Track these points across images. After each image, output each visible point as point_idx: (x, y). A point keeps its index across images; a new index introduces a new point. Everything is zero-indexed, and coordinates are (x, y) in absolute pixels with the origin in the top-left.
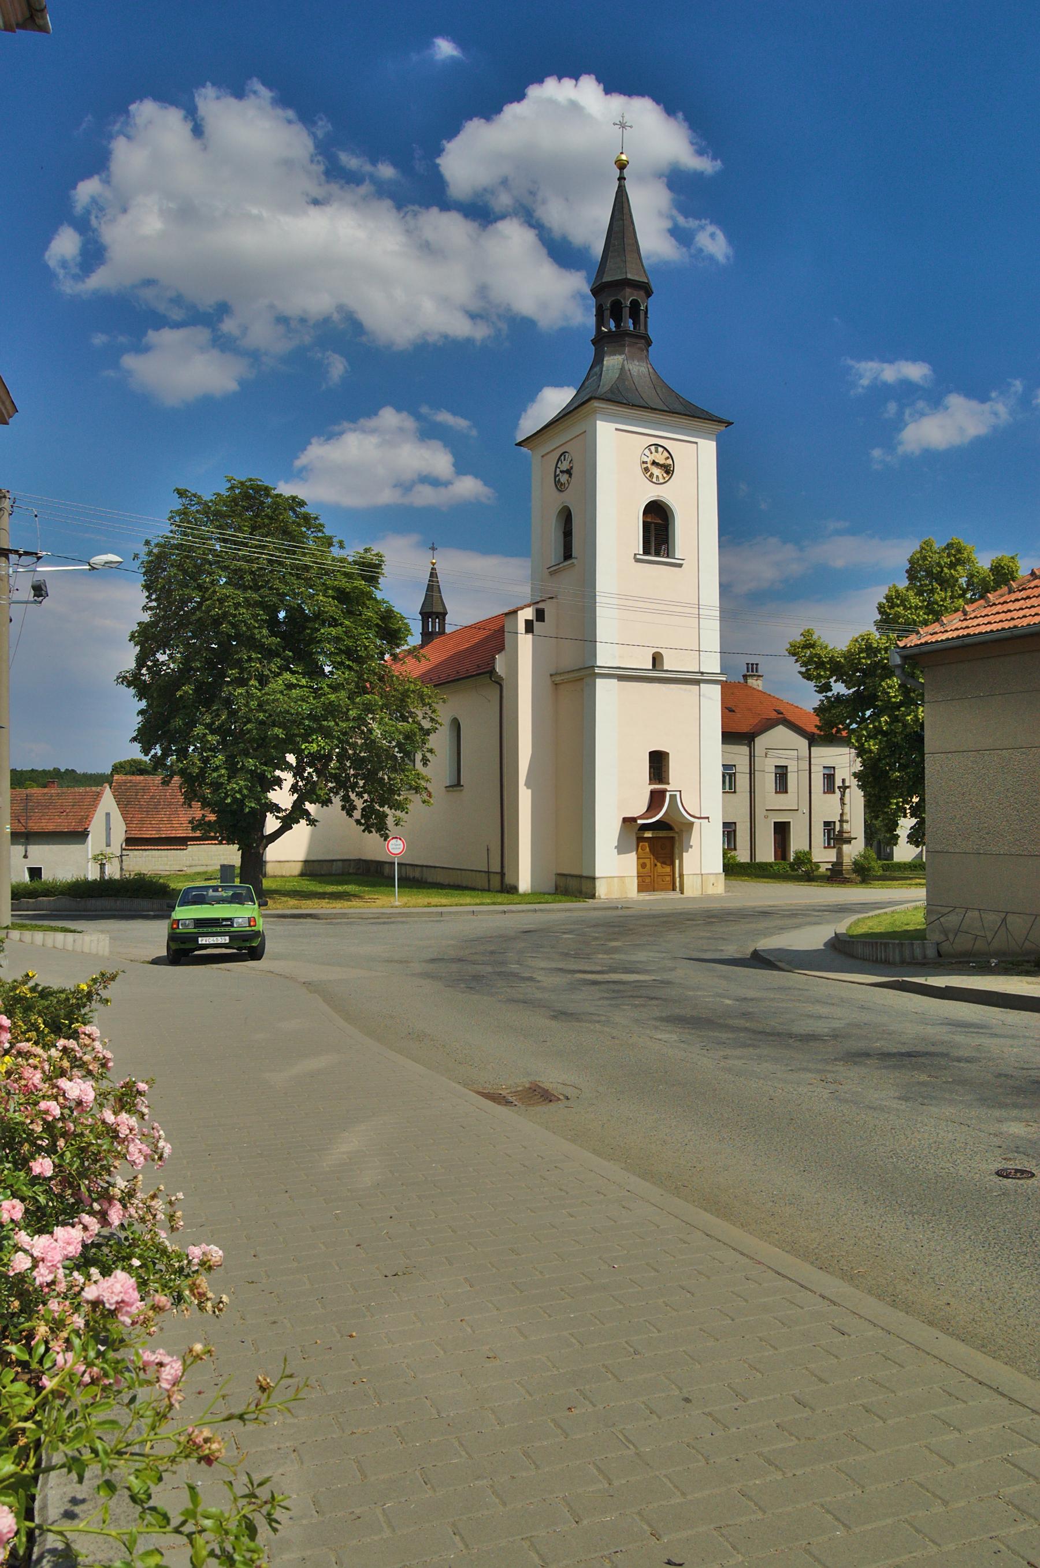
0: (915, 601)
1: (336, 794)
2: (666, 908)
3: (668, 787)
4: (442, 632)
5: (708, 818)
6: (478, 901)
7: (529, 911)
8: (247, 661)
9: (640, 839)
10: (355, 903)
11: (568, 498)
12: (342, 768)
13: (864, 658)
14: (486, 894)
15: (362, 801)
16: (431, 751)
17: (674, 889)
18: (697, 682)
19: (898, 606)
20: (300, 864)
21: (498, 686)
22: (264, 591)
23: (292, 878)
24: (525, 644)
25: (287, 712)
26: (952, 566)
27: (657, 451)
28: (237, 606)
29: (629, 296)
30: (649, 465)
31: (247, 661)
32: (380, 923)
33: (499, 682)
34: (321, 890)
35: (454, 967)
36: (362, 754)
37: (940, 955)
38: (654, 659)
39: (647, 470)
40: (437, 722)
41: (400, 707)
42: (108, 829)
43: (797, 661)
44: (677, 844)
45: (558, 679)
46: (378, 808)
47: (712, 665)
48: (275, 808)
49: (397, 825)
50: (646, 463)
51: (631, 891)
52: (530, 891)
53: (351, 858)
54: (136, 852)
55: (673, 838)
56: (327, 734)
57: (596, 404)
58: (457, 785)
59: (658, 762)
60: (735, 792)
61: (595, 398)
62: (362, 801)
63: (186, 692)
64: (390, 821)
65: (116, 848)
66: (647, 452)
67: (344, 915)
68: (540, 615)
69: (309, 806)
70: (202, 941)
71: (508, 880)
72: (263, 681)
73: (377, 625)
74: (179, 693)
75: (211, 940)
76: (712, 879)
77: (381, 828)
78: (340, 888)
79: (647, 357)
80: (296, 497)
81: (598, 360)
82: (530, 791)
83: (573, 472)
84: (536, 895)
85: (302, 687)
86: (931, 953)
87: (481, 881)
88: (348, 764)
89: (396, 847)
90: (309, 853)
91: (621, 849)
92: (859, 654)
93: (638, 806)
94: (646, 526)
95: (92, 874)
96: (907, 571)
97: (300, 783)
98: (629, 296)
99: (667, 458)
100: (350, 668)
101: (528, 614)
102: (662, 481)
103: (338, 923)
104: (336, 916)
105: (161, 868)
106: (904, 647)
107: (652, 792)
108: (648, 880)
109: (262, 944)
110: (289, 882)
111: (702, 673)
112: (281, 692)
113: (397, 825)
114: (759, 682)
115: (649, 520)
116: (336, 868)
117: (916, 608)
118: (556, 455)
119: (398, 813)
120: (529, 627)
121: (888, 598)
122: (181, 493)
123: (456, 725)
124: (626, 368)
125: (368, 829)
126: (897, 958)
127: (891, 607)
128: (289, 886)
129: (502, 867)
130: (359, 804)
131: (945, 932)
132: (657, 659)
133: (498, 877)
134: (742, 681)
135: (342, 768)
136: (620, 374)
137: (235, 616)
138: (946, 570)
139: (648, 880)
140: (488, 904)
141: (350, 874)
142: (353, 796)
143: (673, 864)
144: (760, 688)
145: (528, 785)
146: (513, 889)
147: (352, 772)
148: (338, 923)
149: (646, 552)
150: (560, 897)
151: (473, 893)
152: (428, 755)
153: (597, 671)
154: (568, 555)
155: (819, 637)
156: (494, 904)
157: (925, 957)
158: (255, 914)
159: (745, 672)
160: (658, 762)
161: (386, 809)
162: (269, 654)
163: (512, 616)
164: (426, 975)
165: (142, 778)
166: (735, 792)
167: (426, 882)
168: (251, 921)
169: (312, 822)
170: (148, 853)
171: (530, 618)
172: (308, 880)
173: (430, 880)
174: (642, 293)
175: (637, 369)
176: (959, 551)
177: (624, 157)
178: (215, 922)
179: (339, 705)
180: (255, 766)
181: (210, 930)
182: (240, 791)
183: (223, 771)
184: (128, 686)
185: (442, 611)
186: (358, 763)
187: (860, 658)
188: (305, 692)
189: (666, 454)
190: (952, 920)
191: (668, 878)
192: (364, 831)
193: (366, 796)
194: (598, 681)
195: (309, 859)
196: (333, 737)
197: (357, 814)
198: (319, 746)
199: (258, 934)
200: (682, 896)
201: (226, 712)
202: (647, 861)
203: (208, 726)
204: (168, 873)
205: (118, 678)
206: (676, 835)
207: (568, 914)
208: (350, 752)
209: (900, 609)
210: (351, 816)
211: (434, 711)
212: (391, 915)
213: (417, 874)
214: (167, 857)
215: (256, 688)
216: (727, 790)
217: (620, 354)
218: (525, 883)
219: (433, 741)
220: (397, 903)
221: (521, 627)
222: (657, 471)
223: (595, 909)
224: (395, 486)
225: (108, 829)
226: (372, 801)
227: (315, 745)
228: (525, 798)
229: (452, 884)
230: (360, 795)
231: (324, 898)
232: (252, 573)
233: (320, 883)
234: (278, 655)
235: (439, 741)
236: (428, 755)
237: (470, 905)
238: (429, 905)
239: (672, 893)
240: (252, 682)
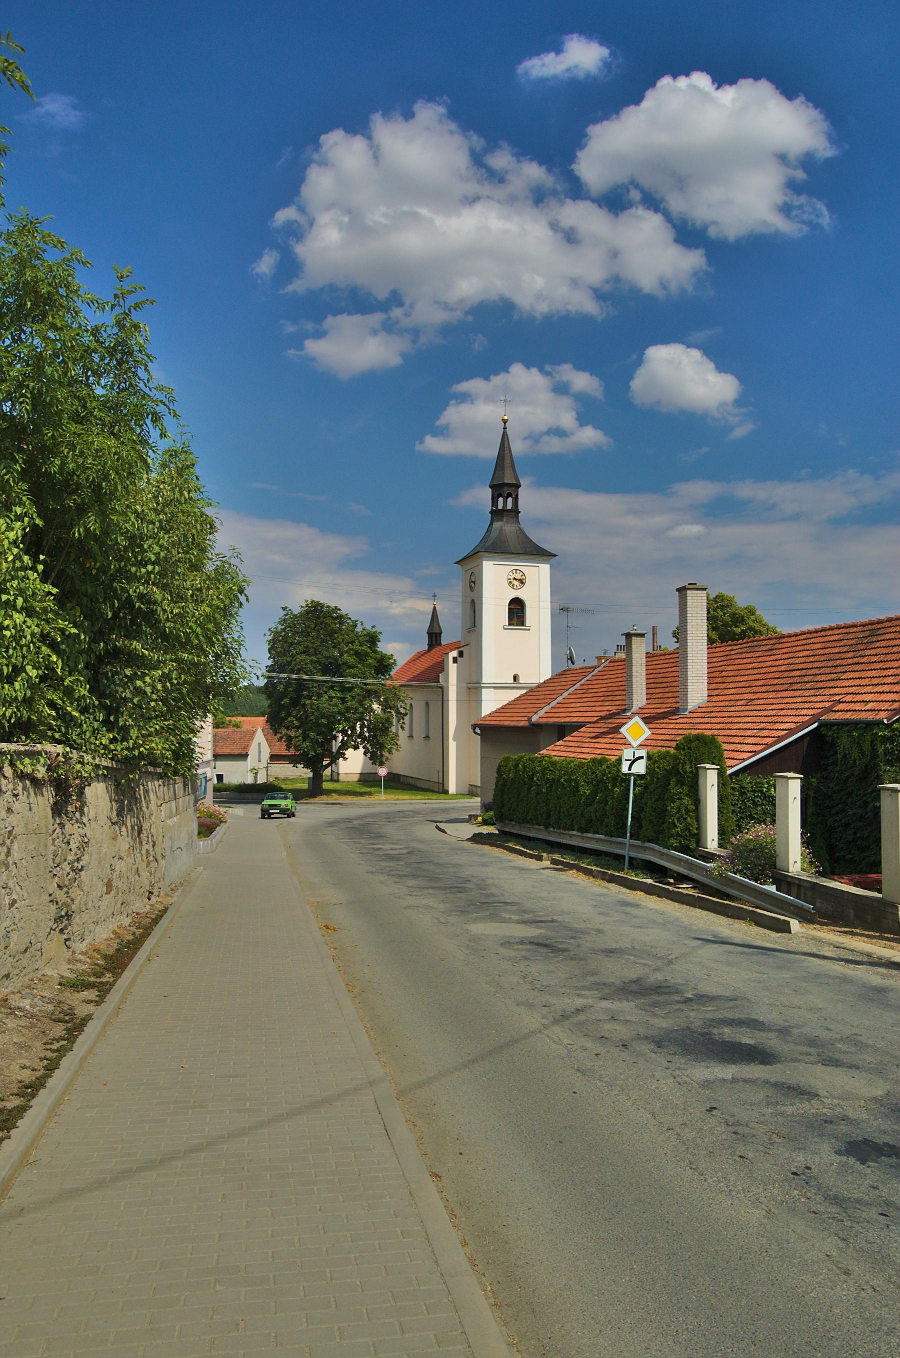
6: (423, 797)
20: (358, 775)
22: (319, 656)
24: (452, 669)
28: (306, 664)
42: (260, 752)
45: (470, 686)
57: (482, 554)
65: (264, 763)
66: (511, 574)
67: (354, 804)
68: (461, 654)
70: (271, 811)
71: (445, 788)
73: (375, 666)
74: (283, 703)
75: (273, 811)
84: (459, 795)
90: (363, 769)
94: (510, 610)
95: (250, 780)
101: (454, 654)
104: (351, 804)
105: (290, 774)
118: (470, 572)
122: (284, 609)
132: (515, 678)
145: (454, 739)
146: (446, 792)
149: (509, 625)
153: (482, 685)
171: (456, 656)
177: (506, 418)
182: (307, 748)
188: (339, 701)
194: (483, 690)
203: (295, 717)
213: (412, 782)
218: (452, 788)
221: (451, 660)
222: (516, 583)
224: (525, 439)
225: (260, 752)
232: (314, 648)
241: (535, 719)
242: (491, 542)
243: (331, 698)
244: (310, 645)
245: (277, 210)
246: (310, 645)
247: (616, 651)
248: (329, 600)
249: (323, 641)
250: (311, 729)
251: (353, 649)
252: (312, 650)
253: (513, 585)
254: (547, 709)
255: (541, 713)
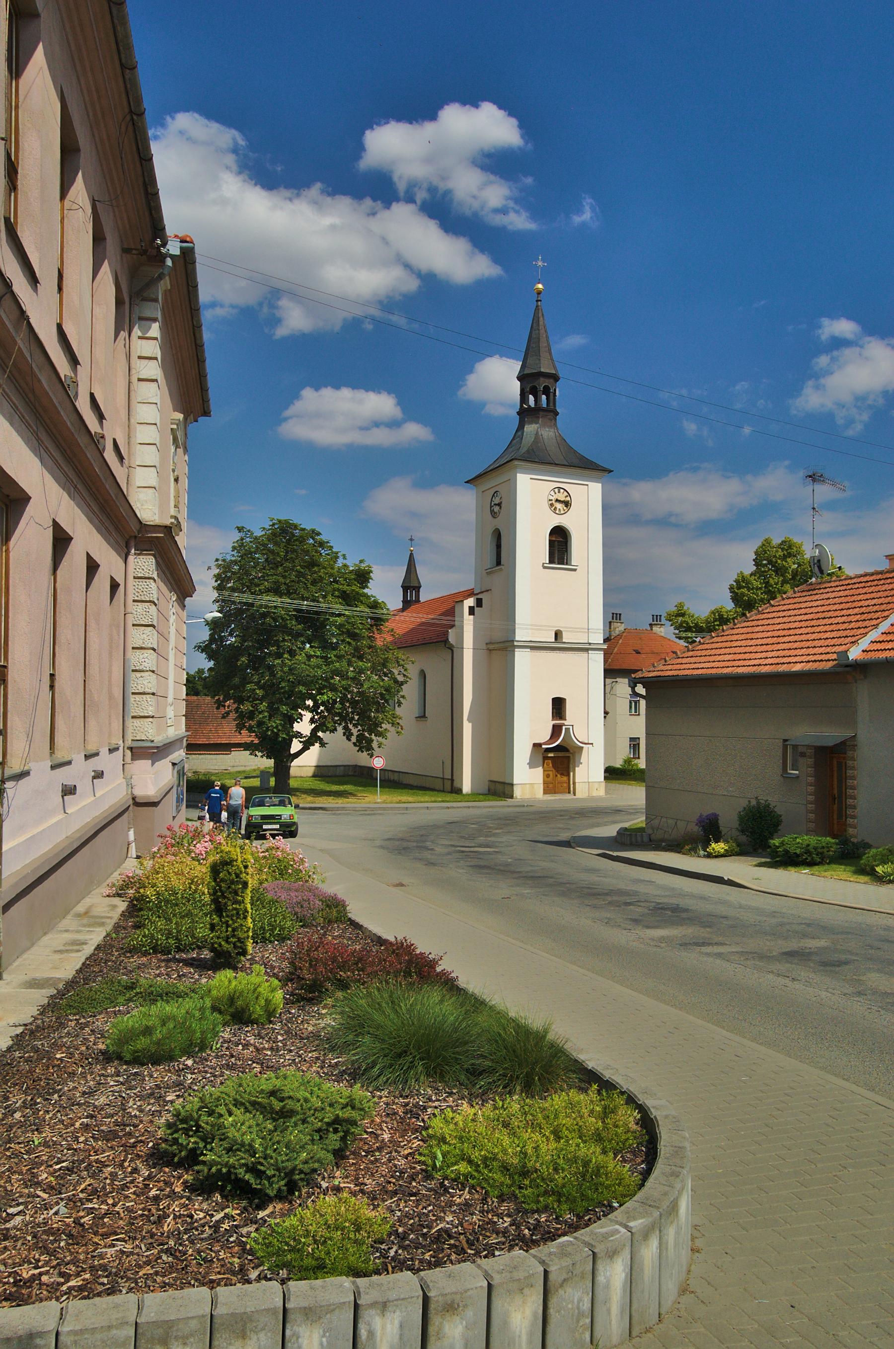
0: (757, 584)
1: (340, 724)
2: (558, 806)
3: (566, 723)
4: (418, 601)
5: (592, 744)
6: (433, 799)
7: (465, 807)
8: (282, 641)
9: (545, 758)
10: (351, 800)
11: (499, 523)
12: (344, 708)
13: (717, 625)
14: (441, 794)
15: (357, 729)
16: (403, 697)
17: (569, 793)
18: (587, 650)
19: (744, 587)
21: (450, 651)
23: (308, 779)
24: (468, 623)
25: (308, 676)
26: (784, 558)
27: (559, 492)
29: (542, 383)
30: (553, 502)
31: (282, 641)
32: (366, 815)
33: (451, 648)
34: (328, 789)
35: (397, 843)
36: (357, 699)
37: (650, 840)
38: (556, 635)
39: (552, 505)
40: (407, 677)
41: (381, 667)
43: (672, 625)
44: (571, 761)
45: (491, 647)
46: (368, 735)
47: (598, 638)
48: (298, 735)
49: (379, 747)
50: (551, 500)
51: (539, 793)
52: (470, 792)
53: (349, 764)
54: (194, 756)
55: (569, 757)
56: (333, 689)
57: (516, 463)
58: (422, 716)
59: (559, 705)
60: (639, 715)
61: (516, 459)
62: (357, 729)
63: (243, 662)
64: (375, 745)
66: (552, 493)
68: (479, 603)
69: (320, 734)
70: (265, 827)
71: (456, 784)
72: (292, 653)
74: (239, 663)
76: (596, 786)
77: (369, 748)
78: (341, 787)
79: (555, 425)
80: (315, 530)
81: (521, 427)
82: (470, 724)
83: (503, 505)
84: (475, 795)
85: (317, 657)
86: (646, 839)
87: (438, 784)
88: (348, 705)
89: (378, 763)
91: (532, 765)
92: (714, 622)
93: (544, 735)
94: (551, 543)
96: (754, 560)
97: (316, 717)
98: (542, 383)
99: (566, 496)
100: (349, 643)
101: (470, 602)
102: (562, 512)
103: (340, 814)
104: (338, 809)
105: (213, 767)
106: (635, 678)
107: (554, 726)
108: (551, 786)
109: (297, 829)
110: (306, 781)
111: (590, 644)
112: (305, 663)
113: (379, 747)
114: (662, 629)
115: (554, 539)
116: (339, 771)
117: (757, 589)
119: (380, 739)
120: (472, 611)
121: (737, 581)
122: (240, 529)
123: (423, 675)
124: (540, 434)
125: (361, 750)
126: (628, 842)
127: (739, 588)
128: (307, 785)
129: (452, 775)
130: (355, 731)
131: (653, 829)
132: (558, 635)
133: (450, 782)
134: (649, 628)
135: (344, 708)
136: (535, 438)
137: (274, 613)
138: (779, 561)
139: (551, 786)
140: (440, 802)
141: (349, 776)
142: (350, 726)
143: (569, 775)
144: (663, 634)
145: (469, 720)
146: (459, 791)
147: (350, 710)
148: (340, 814)
149: (551, 562)
150: (490, 797)
151: (431, 793)
152: (401, 699)
153: (516, 644)
154: (499, 563)
155: (688, 609)
156: (443, 801)
157: (642, 841)
158: (293, 813)
159: (651, 622)
160: (559, 705)
161: (373, 736)
162: (297, 635)
163: (460, 603)
164: (382, 847)
165: (195, 698)
166: (639, 715)
167: (402, 784)
168: (291, 816)
169: (323, 744)
170: (202, 756)
172: (319, 780)
173: (405, 782)
174: (552, 380)
175: (547, 433)
176: (790, 547)
178: (272, 817)
179: (342, 671)
180: (287, 710)
181: (269, 821)
182: (277, 727)
183: (266, 714)
184: (202, 652)
185: (417, 585)
186: (354, 703)
187: (714, 625)
188: (320, 661)
189: (566, 494)
190: (656, 822)
191: (565, 785)
192: (358, 751)
193: (360, 727)
195: (321, 764)
196: (338, 691)
197: (354, 739)
198: (328, 697)
199: (294, 824)
200: (575, 797)
201: (268, 673)
202: (550, 773)
203: (257, 683)
204: (217, 771)
205: (195, 648)
206: (571, 755)
207: (490, 810)
208: (349, 696)
209: (745, 591)
210: (350, 740)
211: (406, 670)
212: (373, 809)
213: (395, 777)
214: (216, 759)
215: (288, 659)
216: (633, 713)
217: (536, 423)
218: (467, 787)
219: (406, 690)
220: (379, 800)
221: (466, 611)
222: (559, 506)
223: (509, 806)
226: (363, 730)
227: (325, 697)
228: (467, 729)
229: (419, 785)
230: (355, 726)
231: (330, 796)
233: (328, 783)
234: (302, 635)
235: (410, 691)
236: (401, 699)
237: (427, 802)
238: (400, 802)
239: (568, 795)
240: (286, 656)
241: (854, 654)
242: (525, 449)
243: (309, 657)
244: (282, 580)
245: (186, 110)
246: (282, 580)
247: (611, 620)
248: (305, 521)
249: (300, 574)
250: (281, 701)
251: (338, 590)
252: (283, 587)
253: (555, 509)
254: (874, 635)
255: (864, 643)
